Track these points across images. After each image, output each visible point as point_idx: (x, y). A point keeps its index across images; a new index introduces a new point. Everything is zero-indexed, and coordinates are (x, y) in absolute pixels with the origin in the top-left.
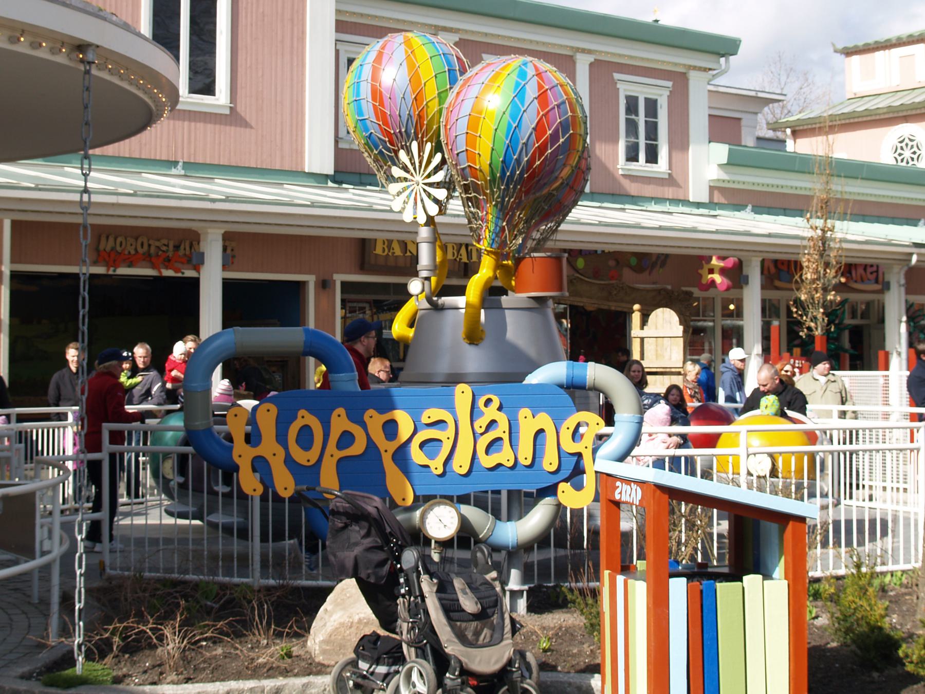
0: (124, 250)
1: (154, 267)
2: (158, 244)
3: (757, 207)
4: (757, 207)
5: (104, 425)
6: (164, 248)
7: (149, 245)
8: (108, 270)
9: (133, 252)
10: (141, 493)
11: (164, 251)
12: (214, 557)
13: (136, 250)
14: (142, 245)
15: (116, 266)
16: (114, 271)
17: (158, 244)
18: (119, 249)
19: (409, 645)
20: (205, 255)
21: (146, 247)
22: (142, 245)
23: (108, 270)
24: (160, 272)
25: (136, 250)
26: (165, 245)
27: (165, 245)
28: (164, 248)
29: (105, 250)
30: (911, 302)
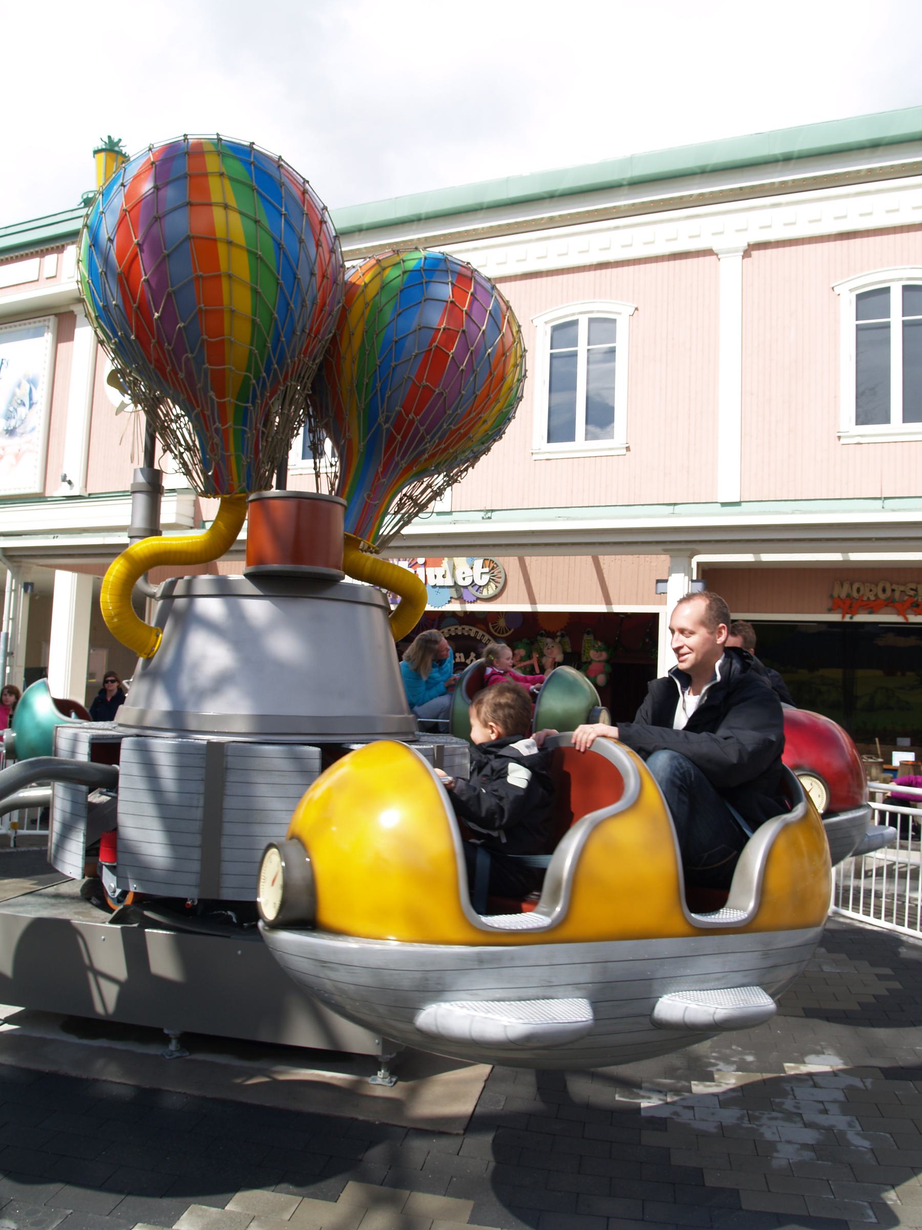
0: (863, 596)
1: (899, 613)
2: (902, 588)
3: (75, 815)
4: (75, 815)
5: (895, 753)
6: (912, 593)
7: (893, 590)
8: (843, 617)
9: (872, 598)
10: (188, 347)
11: (911, 596)
12: (903, 876)
13: (876, 595)
14: (884, 590)
15: (853, 613)
16: (851, 618)
17: (902, 588)
18: (855, 595)
19: (432, 491)
20: (332, 1204)
21: (889, 592)
22: (884, 590)
23: (843, 617)
24: (906, 619)
25: (876, 595)
26: (912, 589)
27: (912, 589)
28: (912, 593)
29: (839, 597)
30: (546, 746)
